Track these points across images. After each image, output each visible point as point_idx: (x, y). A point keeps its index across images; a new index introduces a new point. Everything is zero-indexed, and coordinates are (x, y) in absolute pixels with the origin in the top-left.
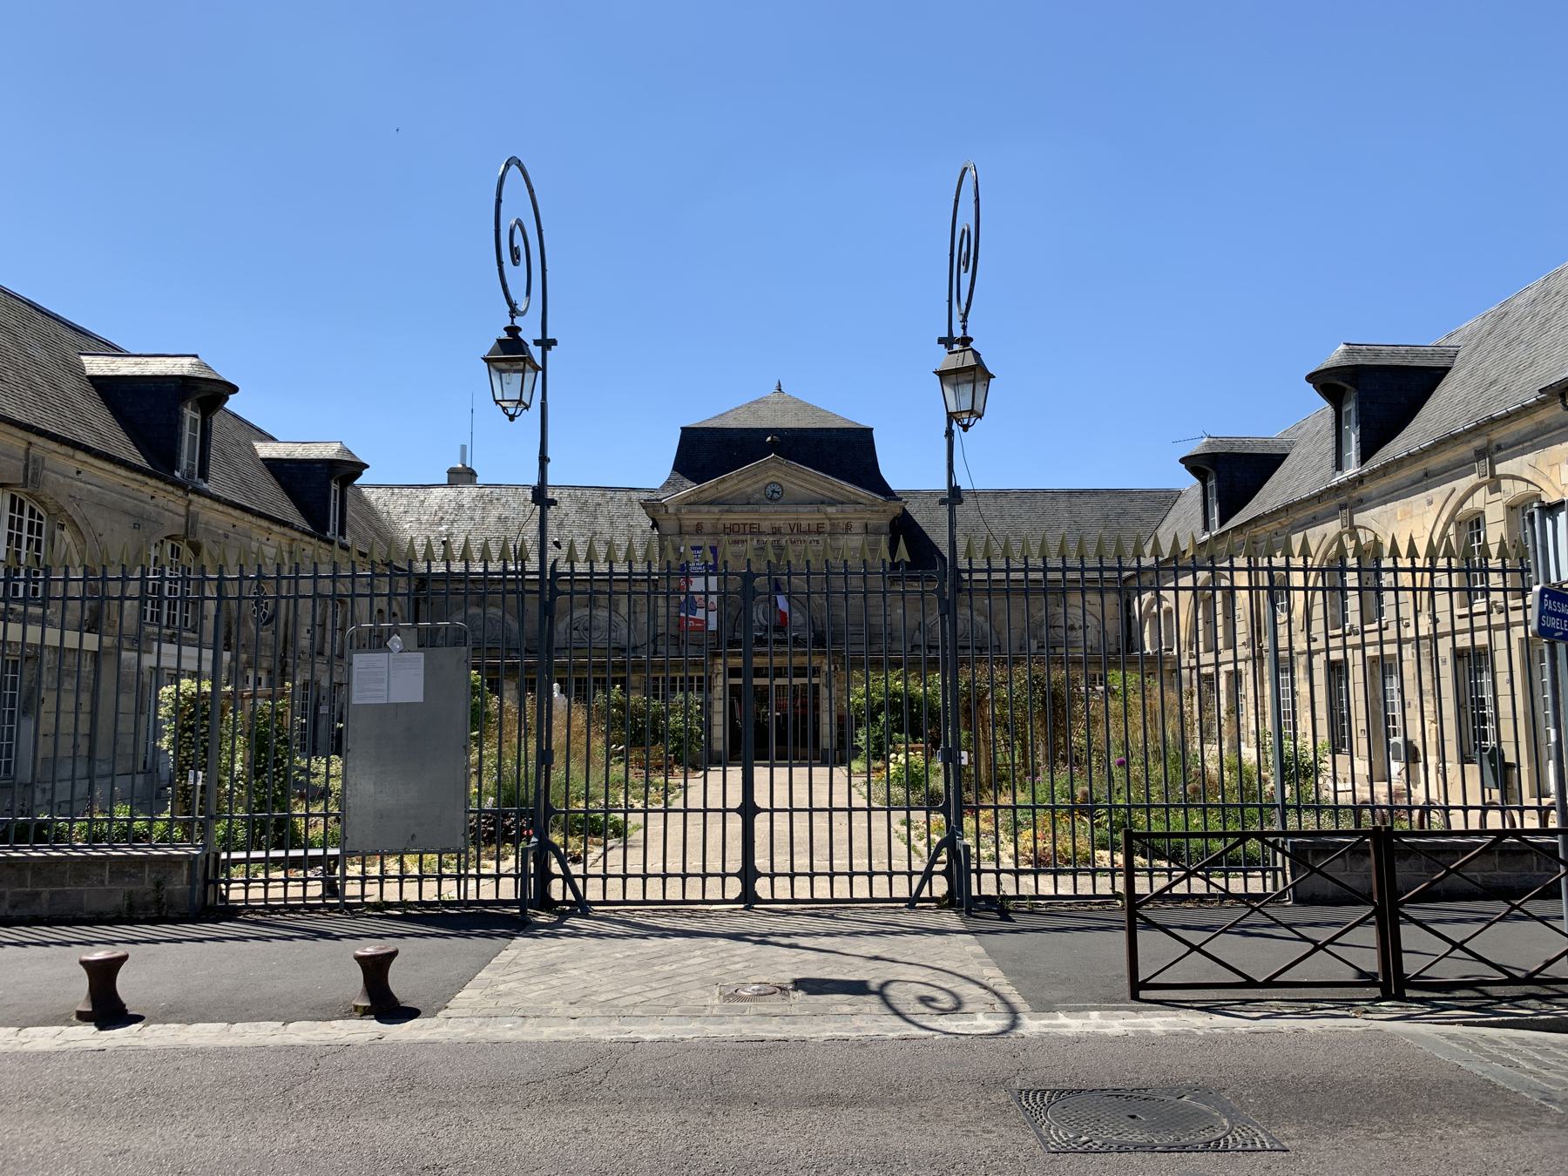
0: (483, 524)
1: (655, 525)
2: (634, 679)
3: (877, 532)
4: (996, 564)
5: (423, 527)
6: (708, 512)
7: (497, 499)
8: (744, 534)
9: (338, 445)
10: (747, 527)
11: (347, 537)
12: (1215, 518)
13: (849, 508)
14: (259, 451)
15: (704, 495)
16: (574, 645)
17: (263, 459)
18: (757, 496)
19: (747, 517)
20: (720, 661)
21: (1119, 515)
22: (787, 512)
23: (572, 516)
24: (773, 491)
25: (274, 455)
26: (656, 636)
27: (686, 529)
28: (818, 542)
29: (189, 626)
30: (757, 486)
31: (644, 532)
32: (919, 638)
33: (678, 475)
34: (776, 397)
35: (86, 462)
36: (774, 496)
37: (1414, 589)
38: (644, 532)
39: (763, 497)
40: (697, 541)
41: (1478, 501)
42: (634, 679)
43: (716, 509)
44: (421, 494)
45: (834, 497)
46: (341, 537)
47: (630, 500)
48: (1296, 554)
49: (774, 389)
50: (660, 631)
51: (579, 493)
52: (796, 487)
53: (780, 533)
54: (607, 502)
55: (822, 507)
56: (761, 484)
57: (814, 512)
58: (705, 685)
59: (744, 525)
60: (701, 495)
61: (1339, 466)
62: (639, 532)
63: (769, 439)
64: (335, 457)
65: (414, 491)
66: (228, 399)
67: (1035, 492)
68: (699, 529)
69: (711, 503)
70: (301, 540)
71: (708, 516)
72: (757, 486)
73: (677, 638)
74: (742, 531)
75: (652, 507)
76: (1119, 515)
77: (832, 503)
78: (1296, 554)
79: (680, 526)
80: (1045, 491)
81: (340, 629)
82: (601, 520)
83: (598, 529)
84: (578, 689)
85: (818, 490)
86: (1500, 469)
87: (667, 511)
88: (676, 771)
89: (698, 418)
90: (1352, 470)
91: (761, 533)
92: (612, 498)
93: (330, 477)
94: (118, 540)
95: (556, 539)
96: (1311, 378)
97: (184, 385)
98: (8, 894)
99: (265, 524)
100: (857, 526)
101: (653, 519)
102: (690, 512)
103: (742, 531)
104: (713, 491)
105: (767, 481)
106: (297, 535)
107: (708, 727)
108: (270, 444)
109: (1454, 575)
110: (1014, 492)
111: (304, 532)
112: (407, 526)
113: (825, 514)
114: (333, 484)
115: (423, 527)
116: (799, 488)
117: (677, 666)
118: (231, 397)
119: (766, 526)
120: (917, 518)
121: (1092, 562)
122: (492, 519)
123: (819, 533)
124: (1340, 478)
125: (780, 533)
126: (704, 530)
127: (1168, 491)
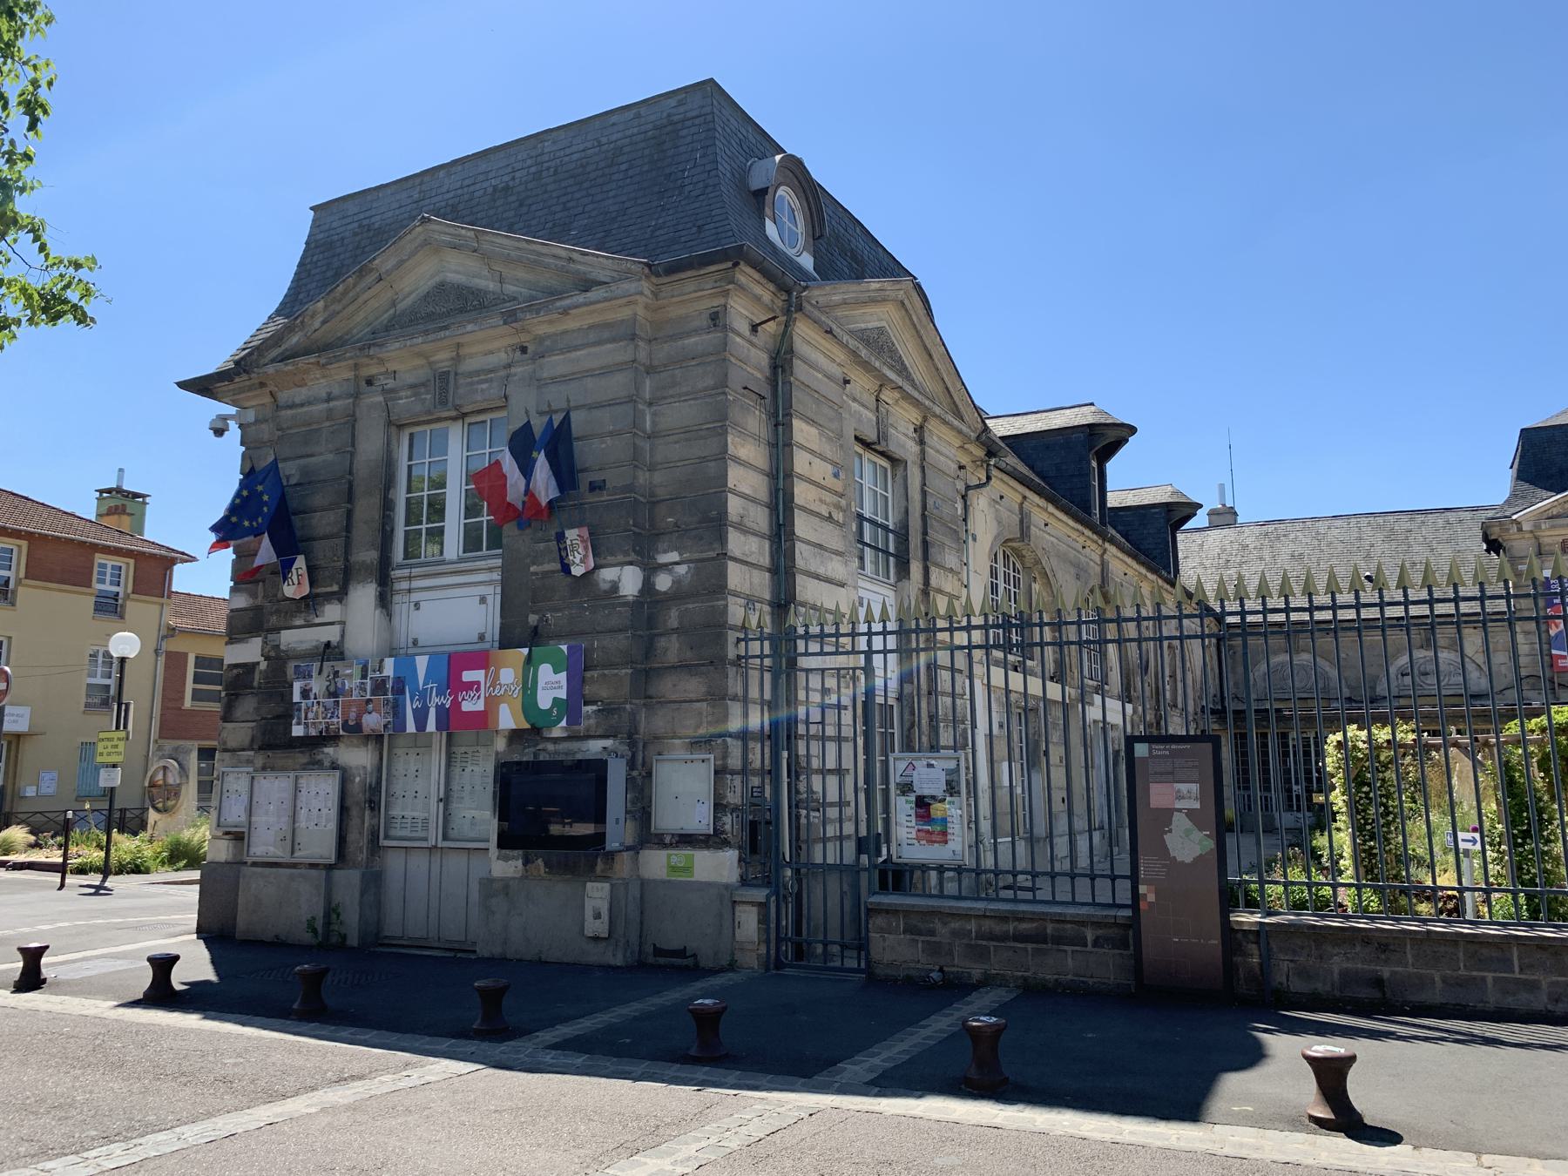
4: (1250, 605)
5: (1209, 571)
9: (1169, 488)
16: (1298, 695)
27: (1547, 548)
33: (1526, 486)
35: (1053, 514)
37: (1202, 637)
42: (1500, 726)
48: (877, 620)
50: (1524, 673)
51: (1380, 520)
64: (1170, 500)
78: (877, 620)
82: (1416, 548)
87: (1520, 530)
89: (1538, 418)
92: (1423, 522)
94: (1070, 592)
95: (1368, 574)
98: (1544, 985)
102: (1553, 527)
109: (1046, 629)
115: (1209, 571)
121: (1299, 601)
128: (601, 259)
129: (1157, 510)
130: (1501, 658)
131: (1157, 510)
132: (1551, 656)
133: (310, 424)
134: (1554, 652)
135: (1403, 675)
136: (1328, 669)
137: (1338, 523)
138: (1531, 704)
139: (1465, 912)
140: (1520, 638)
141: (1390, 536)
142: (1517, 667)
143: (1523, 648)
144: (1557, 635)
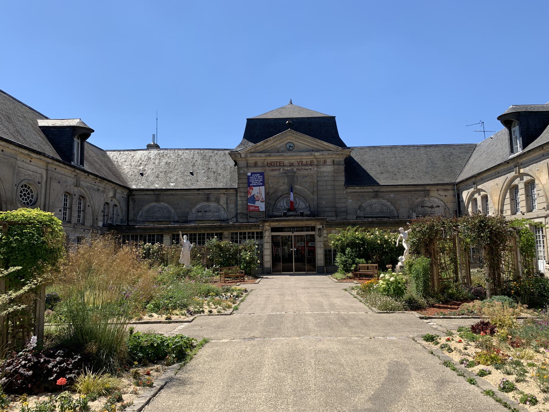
0: (159, 165)
1: (236, 164)
2: (226, 233)
3: (339, 164)
5: (132, 167)
6: (260, 156)
7: (166, 155)
10: (278, 163)
11: (85, 165)
12: (519, 144)
13: (325, 153)
14: (39, 123)
15: (257, 149)
17: (40, 127)
18: (282, 149)
19: (277, 158)
20: (267, 224)
21: (450, 156)
22: (296, 156)
23: (199, 162)
24: (290, 146)
25: (46, 125)
26: (237, 214)
27: (250, 165)
28: (311, 169)
29: (67, 220)
30: (281, 144)
31: (231, 167)
32: (360, 213)
33: (246, 140)
34: (290, 106)
36: (290, 148)
38: (231, 167)
40: (255, 170)
41: (516, 182)
42: (226, 233)
43: (263, 155)
44: (132, 153)
45: (318, 148)
46: (81, 166)
47: (225, 154)
49: (289, 103)
50: (239, 212)
51: (202, 151)
54: (215, 155)
55: (313, 153)
56: (284, 143)
57: (309, 155)
58: (260, 236)
59: (277, 162)
60: (256, 149)
61: (512, 151)
62: (229, 167)
63: (287, 122)
65: (130, 152)
66: (90, 135)
67: (409, 146)
68: (256, 165)
69: (261, 152)
70: (53, 163)
71: (260, 158)
72: (281, 144)
73: (247, 215)
75: (233, 154)
76: (450, 156)
77: (318, 151)
79: (247, 163)
80: (414, 146)
81: (82, 211)
82: (212, 163)
83: (210, 167)
84: (199, 239)
85: (311, 145)
86: (479, 187)
87: (241, 157)
88: (246, 279)
90: (520, 151)
91: (284, 166)
92: (217, 153)
93: (73, 135)
95: (191, 171)
96: (499, 118)
97: (73, 129)
99: (26, 152)
100: (329, 161)
101: (235, 161)
102: (251, 156)
104: (262, 146)
105: (287, 142)
106: (50, 161)
107: (261, 257)
108: (45, 120)
110: (400, 146)
111: (53, 159)
112: (125, 167)
113: (314, 156)
114: (75, 139)
115: (132, 167)
116: (302, 145)
117: (246, 227)
118: (92, 134)
119: (286, 162)
120: (356, 159)
122: (163, 163)
123: (311, 165)
124: (512, 156)
127: (470, 144)
129: (68, 129)
131: (68, 129)
132: (247, 205)
135: (198, 212)
136: (171, 209)
137: (187, 151)
139: (73, 160)
140: (239, 198)
141: (204, 158)
142: (237, 209)
143: (239, 203)
144: (250, 197)
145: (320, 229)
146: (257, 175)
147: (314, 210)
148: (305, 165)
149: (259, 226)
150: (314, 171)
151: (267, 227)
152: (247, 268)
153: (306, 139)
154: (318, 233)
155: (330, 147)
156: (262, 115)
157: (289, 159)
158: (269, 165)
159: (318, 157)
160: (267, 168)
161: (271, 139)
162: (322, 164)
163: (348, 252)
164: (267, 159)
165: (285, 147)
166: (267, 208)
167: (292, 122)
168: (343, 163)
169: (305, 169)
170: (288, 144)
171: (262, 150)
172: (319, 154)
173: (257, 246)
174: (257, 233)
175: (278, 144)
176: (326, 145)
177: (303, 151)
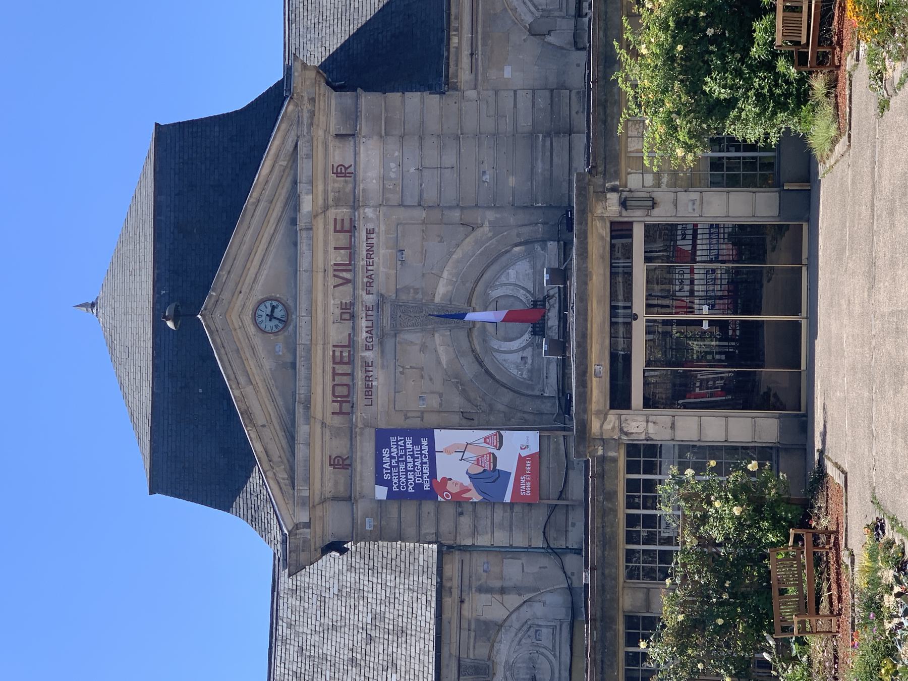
1: (338, 546)
8: (352, 375)
10: (340, 369)
13: (304, 168)
15: (275, 453)
18: (280, 348)
20: (595, 426)
22: (310, 291)
24: (271, 317)
27: (341, 488)
28: (370, 232)
31: (351, 568)
32: (561, 36)
33: (240, 501)
38: (351, 568)
39: (281, 337)
43: (302, 430)
47: (294, 591)
50: (539, 542)
52: (264, 273)
53: (352, 304)
54: (297, 634)
56: (258, 340)
57: (311, 238)
59: (335, 374)
60: (276, 458)
62: (350, 577)
63: (170, 324)
68: (342, 463)
69: (291, 438)
74: (346, 380)
77: (293, 201)
79: (334, 499)
82: (328, 649)
87: (308, 525)
91: (351, 344)
92: (290, 626)
100: (340, 155)
101: (328, 548)
102: (308, 481)
103: (346, 380)
105: (252, 329)
119: (337, 333)
120: (334, 44)
125: (352, 304)
126: (344, 452)
128: (272, 487)
130: (513, 570)
132: (512, 505)
133: (362, 463)
134: (508, 498)
138: (586, 585)
140: (483, 540)
142: (528, 550)
143: (501, 538)
145: (624, 204)
146: (386, 459)
147: (544, 223)
148: (352, 257)
149: (603, 459)
150: (378, 218)
151: (608, 426)
152: (781, 518)
153: (245, 248)
154: (638, 213)
155: (279, 150)
156: (136, 427)
157: (325, 321)
158: (346, 407)
159: (320, 202)
160: (360, 415)
161: (237, 393)
162: (350, 186)
163: (725, 87)
164: (319, 416)
165: (272, 337)
166: (526, 421)
167: (173, 306)
168: (347, 97)
169: (369, 257)
170: (263, 326)
171: (281, 434)
172: (310, 197)
173: (689, 472)
174: (632, 467)
175: (261, 367)
176: (273, 166)
177: (293, 262)
